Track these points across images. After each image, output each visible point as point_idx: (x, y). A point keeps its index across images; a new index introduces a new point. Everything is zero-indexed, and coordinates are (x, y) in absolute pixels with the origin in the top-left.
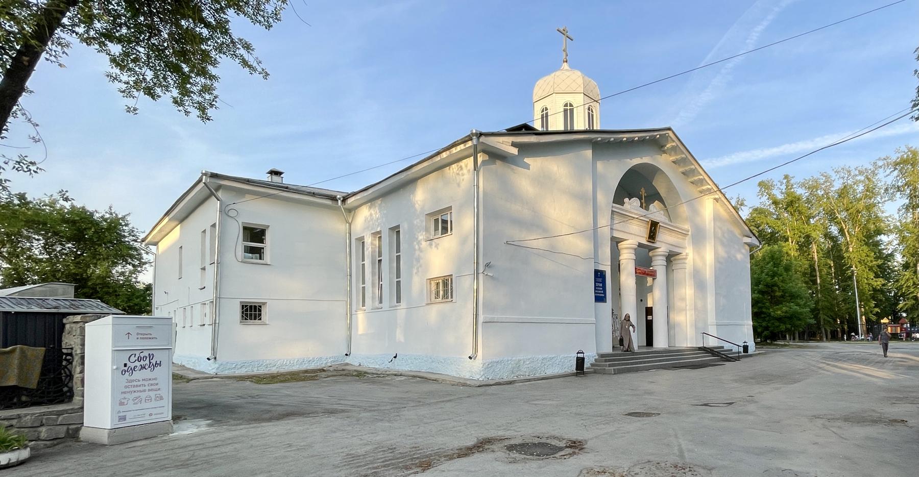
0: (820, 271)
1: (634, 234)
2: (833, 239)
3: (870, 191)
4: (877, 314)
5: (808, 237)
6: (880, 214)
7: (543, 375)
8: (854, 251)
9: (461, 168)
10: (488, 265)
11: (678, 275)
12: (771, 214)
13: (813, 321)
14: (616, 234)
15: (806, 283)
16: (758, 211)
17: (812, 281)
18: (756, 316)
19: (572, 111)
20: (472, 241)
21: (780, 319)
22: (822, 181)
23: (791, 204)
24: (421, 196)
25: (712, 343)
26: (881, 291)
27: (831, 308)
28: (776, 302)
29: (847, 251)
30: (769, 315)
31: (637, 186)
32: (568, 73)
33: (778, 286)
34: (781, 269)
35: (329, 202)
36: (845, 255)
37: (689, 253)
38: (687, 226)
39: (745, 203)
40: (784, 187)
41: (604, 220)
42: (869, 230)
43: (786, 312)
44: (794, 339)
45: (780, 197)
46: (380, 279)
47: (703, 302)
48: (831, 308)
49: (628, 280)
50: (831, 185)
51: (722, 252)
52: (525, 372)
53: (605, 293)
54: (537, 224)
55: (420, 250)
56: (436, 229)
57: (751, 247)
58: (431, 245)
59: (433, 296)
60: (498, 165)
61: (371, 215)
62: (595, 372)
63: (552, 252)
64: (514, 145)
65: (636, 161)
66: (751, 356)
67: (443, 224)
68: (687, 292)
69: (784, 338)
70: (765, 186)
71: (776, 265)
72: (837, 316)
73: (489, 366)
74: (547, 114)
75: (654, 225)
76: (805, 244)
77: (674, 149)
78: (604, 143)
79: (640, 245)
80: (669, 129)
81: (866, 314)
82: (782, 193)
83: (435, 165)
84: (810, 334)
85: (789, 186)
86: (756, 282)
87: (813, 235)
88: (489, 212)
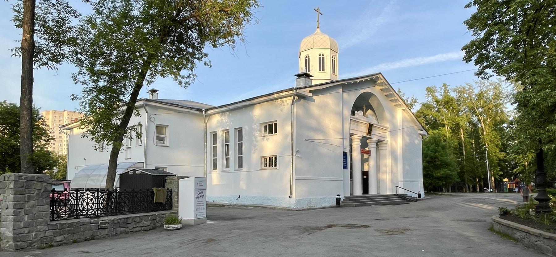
0: (465, 147)
1: (362, 131)
2: (475, 125)
3: (497, 96)
4: (501, 176)
5: (458, 124)
6: (504, 110)
7: (320, 206)
8: (487, 134)
9: (283, 102)
10: (297, 152)
11: (382, 152)
12: (434, 107)
13: (459, 180)
14: (352, 132)
15: (457, 154)
16: (426, 106)
17: (460, 153)
18: (425, 176)
19: (323, 58)
20: (289, 139)
21: (439, 178)
22: (467, 89)
23: (448, 103)
24: (258, 112)
25: (401, 192)
26: (504, 161)
27: (472, 171)
28: (438, 167)
29: (482, 134)
30: (433, 176)
31: (362, 104)
32: (321, 37)
33: (438, 158)
34: (440, 148)
35: (198, 112)
36: (482, 137)
37: (388, 139)
38: (388, 125)
39: (417, 101)
40: (443, 91)
41: (347, 126)
42: (496, 121)
43: (443, 174)
44: (448, 191)
45: (440, 97)
46: (228, 154)
47: (397, 169)
48: (472, 171)
49: (356, 155)
50: (472, 92)
51: (407, 138)
52: (313, 205)
53: (347, 164)
54: (319, 129)
55: (257, 141)
56: (265, 130)
57: (423, 136)
58: (263, 139)
59: (263, 165)
60: (302, 101)
61: (222, 120)
62: (345, 206)
63: (327, 143)
64: (310, 92)
65: (362, 91)
66: (422, 199)
67: (271, 128)
68: (388, 161)
69: (442, 190)
70: (430, 91)
71: (437, 145)
72: (476, 176)
73: (298, 201)
74: (309, 59)
75: (371, 126)
76: (456, 129)
77: (382, 84)
78: (347, 85)
79: (363, 137)
80: (380, 73)
81: (494, 175)
82: (441, 95)
83: (270, 98)
84: (458, 188)
85: (446, 91)
86: (425, 156)
87: (461, 123)
88: (300, 125)
